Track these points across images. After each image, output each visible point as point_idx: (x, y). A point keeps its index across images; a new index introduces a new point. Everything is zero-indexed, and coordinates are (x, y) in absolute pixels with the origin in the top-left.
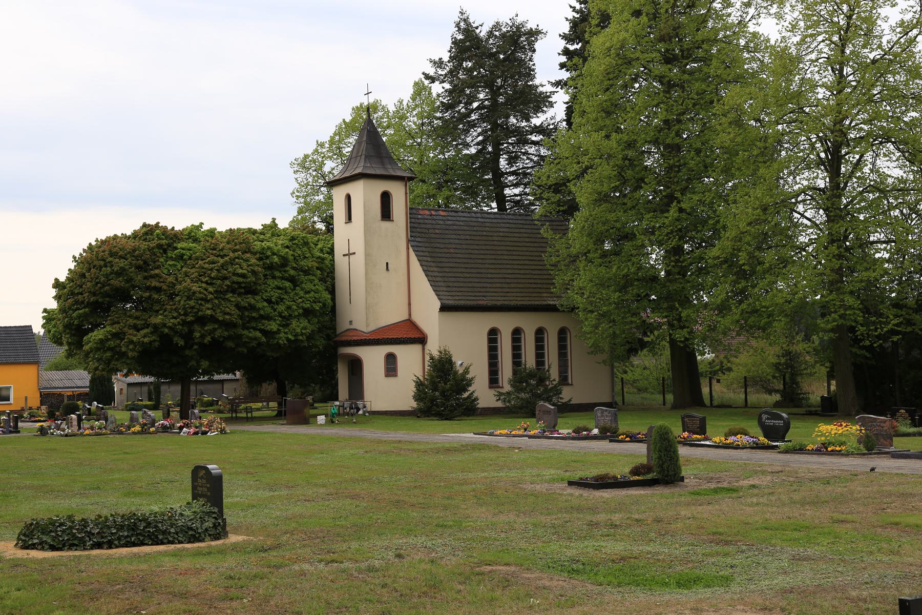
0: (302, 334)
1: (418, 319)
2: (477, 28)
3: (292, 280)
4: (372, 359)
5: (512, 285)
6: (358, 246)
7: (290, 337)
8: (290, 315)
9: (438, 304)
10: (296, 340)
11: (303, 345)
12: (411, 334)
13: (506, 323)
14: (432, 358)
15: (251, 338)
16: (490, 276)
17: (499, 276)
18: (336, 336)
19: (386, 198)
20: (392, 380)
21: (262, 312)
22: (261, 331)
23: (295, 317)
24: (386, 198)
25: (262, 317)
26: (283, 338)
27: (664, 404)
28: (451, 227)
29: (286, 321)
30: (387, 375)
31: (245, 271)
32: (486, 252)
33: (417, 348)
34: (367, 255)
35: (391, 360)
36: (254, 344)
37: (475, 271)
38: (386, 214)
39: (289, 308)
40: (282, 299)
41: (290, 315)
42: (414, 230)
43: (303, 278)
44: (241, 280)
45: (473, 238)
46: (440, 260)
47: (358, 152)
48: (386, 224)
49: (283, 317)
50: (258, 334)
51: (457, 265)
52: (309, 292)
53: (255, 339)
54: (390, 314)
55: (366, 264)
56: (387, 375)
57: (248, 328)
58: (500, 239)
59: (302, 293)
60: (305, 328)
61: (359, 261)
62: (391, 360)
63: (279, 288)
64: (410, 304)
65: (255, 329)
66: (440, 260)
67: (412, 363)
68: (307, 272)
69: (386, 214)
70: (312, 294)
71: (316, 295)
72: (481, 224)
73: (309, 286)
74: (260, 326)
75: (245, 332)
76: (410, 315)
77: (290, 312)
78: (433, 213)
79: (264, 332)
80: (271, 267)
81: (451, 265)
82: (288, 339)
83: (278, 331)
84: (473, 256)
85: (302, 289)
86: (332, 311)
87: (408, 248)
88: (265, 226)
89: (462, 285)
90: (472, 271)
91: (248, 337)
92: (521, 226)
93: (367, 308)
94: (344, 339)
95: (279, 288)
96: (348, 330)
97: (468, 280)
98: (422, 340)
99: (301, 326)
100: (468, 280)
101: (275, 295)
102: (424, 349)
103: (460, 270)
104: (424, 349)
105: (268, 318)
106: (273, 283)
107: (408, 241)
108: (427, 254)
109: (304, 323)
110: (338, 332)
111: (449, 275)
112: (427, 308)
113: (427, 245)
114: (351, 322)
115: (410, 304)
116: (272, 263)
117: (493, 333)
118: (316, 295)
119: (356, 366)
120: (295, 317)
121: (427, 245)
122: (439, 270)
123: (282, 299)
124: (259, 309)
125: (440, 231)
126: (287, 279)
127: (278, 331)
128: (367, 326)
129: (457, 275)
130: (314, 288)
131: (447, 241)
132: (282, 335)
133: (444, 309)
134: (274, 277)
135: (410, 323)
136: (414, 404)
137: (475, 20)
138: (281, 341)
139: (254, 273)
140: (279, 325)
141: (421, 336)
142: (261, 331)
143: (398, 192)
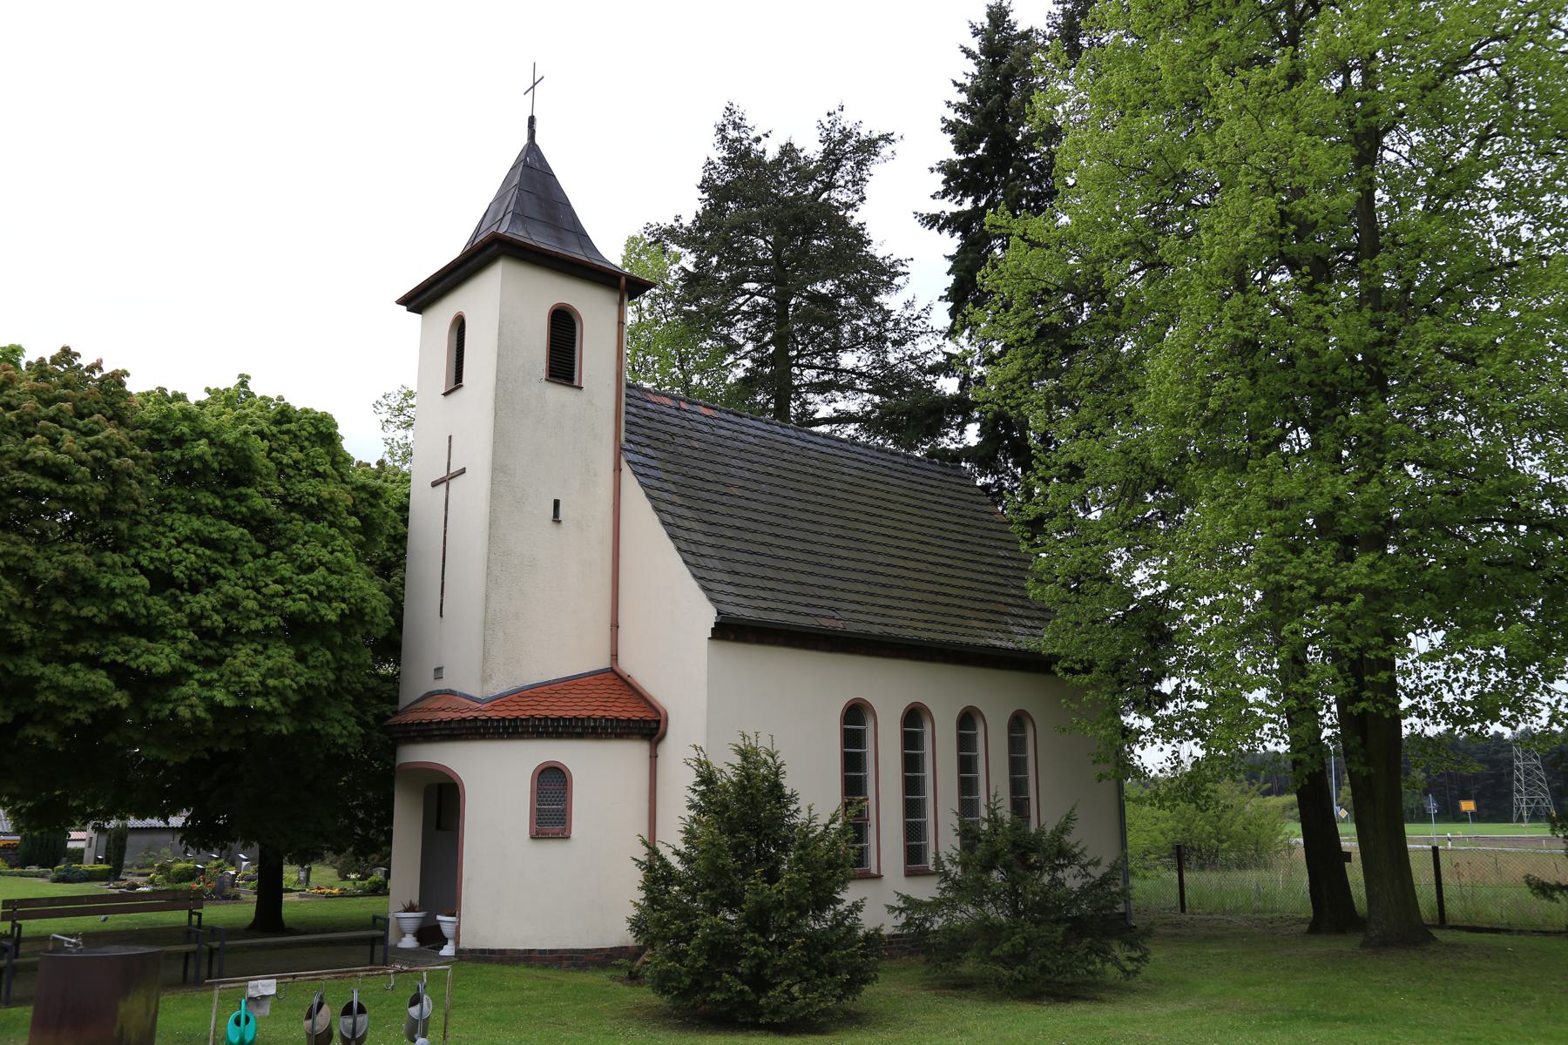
0: (266, 692)
1: (627, 666)
2: (758, 140)
3: (259, 524)
4: (494, 779)
5: (896, 593)
6: (476, 454)
7: (219, 695)
8: (230, 630)
9: (708, 616)
10: (242, 710)
11: (271, 728)
12: (620, 712)
13: (888, 688)
14: (707, 778)
15: (71, 694)
16: (837, 562)
17: (860, 566)
18: (396, 713)
19: (563, 325)
20: (551, 850)
21: (121, 605)
22: (112, 668)
23: (252, 636)
24: (563, 325)
25: (126, 625)
26: (189, 701)
27: (1183, 909)
28: (729, 443)
29: (215, 642)
30: (537, 835)
31: (66, 459)
32: (820, 509)
33: (632, 753)
34: (499, 470)
35: (552, 789)
36: (81, 713)
37: (799, 545)
38: (562, 363)
39: (232, 604)
40: (213, 579)
41: (230, 630)
42: (634, 429)
43: (298, 525)
44: (45, 484)
45: (784, 474)
46: (706, 506)
47: (496, 215)
48: (558, 394)
49: (206, 634)
50: (100, 679)
51: (752, 526)
52: (310, 569)
53: (86, 695)
54: (558, 652)
55: (494, 494)
56: (537, 835)
57: (66, 660)
58: (846, 487)
59: (286, 570)
60: (280, 673)
61: (472, 495)
62: (552, 789)
63: (207, 542)
64: (615, 626)
65: (93, 663)
66: (706, 506)
67: (630, 812)
68: (314, 512)
69: (562, 363)
70: (321, 572)
71: (334, 580)
72: (798, 451)
73: (315, 551)
74: (113, 653)
75: (53, 672)
76: (615, 656)
77: (233, 618)
78: (683, 405)
79: (123, 675)
80: (188, 475)
81: (738, 523)
82: (214, 707)
83: (177, 677)
84: (790, 513)
85: (292, 559)
86: (391, 645)
87: (618, 469)
88: (214, 394)
89: (770, 573)
90: (793, 544)
91: (55, 687)
92: (886, 471)
93: (487, 625)
94: (411, 718)
95: (207, 542)
96: (430, 695)
97: (784, 564)
98: (647, 727)
99: (263, 670)
100: (784, 564)
101: (187, 560)
102: (654, 757)
103: (760, 538)
104: (654, 757)
105: (152, 631)
106: (185, 524)
107: (620, 450)
108: (672, 487)
109: (282, 655)
110: (402, 704)
111: (735, 545)
112: (669, 629)
113: (670, 467)
114: (438, 671)
115: (615, 626)
116: (187, 462)
117: (856, 714)
118: (334, 580)
119: (444, 799)
120: (252, 636)
121: (670, 467)
122: (705, 528)
123: (213, 579)
124: (112, 594)
125: (703, 446)
126: (243, 522)
127: (177, 677)
128: (485, 679)
129: (756, 548)
130: (327, 557)
131: (719, 468)
132: (190, 688)
133: (726, 630)
134: (195, 510)
135: (615, 679)
136: (618, 934)
137: (757, 121)
138: (183, 711)
139: (101, 468)
140: (185, 657)
141: (649, 716)
142: (112, 668)
143: (596, 312)
